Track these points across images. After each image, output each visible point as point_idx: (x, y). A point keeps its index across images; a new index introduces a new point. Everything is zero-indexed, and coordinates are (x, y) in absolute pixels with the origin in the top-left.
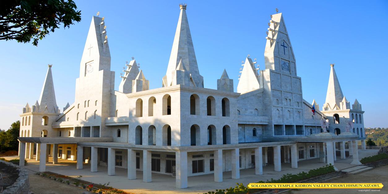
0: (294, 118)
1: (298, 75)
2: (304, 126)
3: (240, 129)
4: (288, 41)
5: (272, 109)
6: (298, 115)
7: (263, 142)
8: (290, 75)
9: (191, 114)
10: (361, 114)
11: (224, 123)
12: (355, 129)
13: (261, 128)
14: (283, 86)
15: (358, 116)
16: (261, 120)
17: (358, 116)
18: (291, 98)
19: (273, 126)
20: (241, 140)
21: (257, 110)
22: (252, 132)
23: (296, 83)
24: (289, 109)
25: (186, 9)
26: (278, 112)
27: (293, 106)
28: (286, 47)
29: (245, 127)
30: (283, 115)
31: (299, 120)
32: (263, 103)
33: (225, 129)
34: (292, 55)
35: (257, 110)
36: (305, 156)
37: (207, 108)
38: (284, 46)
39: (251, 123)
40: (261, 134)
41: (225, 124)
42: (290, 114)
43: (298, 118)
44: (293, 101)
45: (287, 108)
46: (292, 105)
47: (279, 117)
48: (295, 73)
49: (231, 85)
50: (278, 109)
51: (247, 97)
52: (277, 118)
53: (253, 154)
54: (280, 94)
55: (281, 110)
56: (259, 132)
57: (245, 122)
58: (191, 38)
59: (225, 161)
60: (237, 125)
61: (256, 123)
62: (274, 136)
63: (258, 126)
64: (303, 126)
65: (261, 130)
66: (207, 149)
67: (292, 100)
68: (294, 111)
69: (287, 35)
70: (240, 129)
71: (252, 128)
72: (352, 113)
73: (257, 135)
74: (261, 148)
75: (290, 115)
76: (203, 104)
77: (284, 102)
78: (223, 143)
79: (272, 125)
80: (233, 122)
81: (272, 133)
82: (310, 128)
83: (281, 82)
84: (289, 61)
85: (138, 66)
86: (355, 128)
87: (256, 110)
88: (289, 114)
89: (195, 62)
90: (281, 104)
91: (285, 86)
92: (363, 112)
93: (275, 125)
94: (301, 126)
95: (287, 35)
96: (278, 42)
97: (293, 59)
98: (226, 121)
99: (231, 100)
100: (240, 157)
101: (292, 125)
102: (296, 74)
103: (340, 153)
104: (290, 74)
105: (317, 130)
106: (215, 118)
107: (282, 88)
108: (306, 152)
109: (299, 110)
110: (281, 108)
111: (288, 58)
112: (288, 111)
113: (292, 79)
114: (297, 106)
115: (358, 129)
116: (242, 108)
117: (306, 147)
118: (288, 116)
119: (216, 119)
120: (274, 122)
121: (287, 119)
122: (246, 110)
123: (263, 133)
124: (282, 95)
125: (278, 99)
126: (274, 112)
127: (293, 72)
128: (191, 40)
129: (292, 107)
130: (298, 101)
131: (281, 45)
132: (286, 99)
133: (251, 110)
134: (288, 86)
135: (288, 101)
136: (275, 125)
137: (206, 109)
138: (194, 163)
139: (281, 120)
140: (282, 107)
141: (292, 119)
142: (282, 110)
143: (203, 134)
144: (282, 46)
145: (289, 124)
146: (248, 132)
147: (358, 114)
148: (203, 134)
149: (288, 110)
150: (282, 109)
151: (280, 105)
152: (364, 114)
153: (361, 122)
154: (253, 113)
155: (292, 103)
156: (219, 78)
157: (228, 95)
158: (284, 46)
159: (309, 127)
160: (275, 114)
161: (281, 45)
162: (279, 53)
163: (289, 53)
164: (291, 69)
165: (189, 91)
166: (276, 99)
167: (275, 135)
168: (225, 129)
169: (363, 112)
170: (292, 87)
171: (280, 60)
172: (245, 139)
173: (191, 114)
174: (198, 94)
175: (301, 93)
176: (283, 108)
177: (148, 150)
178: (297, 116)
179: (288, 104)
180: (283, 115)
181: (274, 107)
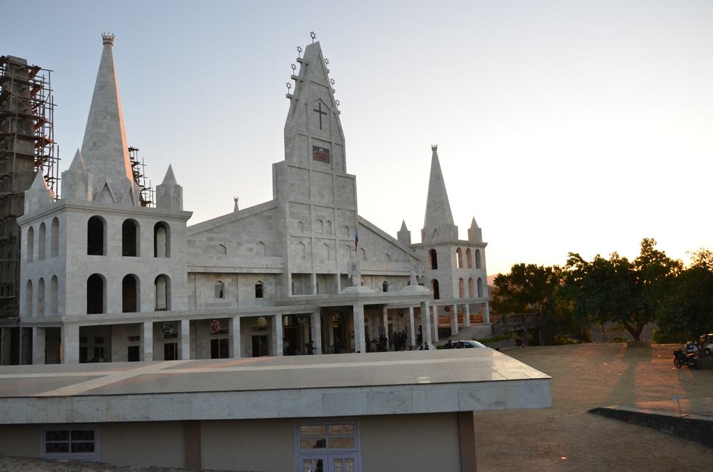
0: (338, 259)
1: (350, 170)
4: (330, 101)
5: (289, 242)
6: (349, 253)
8: (330, 172)
9: (89, 254)
10: (480, 249)
11: (158, 270)
12: (464, 281)
13: (272, 280)
16: (267, 265)
18: (331, 219)
19: (290, 276)
20: (231, 306)
23: (344, 187)
24: (327, 242)
26: (302, 247)
27: (335, 235)
32: (276, 230)
33: (130, 283)
37: (121, 242)
38: (321, 112)
40: (274, 292)
42: (328, 250)
44: (336, 225)
45: (322, 240)
46: (333, 232)
47: (304, 257)
48: (341, 167)
49: (176, 196)
52: (299, 261)
53: (134, 344)
54: (306, 212)
56: (269, 289)
57: (232, 269)
58: (117, 104)
59: (196, 347)
60: (186, 275)
62: (290, 295)
65: (274, 284)
66: (121, 319)
67: (333, 224)
68: (337, 245)
69: (328, 88)
71: (254, 281)
72: (457, 247)
73: (265, 295)
74: (239, 319)
75: (329, 254)
76: (115, 234)
77: (316, 227)
78: (122, 311)
79: (287, 275)
80: (176, 267)
81: (288, 290)
82: (383, 280)
83: (309, 186)
86: (463, 278)
88: (327, 252)
89: (119, 151)
91: (319, 194)
92: (485, 245)
93: (293, 274)
95: (328, 88)
96: (306, 104)
97: (340, 139)
98: (96, 264)
100: (366, 328)
101: (331, 273)
102: (344, 168)
103: (451, 331)
104: (332, 169)
105: (400, 283)
106: (139, 262)
107: (312, 198)
108: (374, 330)
109: (348, 243)
112: (324, 246)
113: (335, 180)
114: (344, 235)
117: (373, 319)
118: (325, 256)
119: (140, 263)
120: (292, 269)
121: (322, 262)
122: (239, 244)
124: (310, 213)
125: (303, 222)
126: (292, 248)
127: (337, 164)
128: (117, 109)
130: (347, 224)
132: (322, 221)
133: (250, 246)
135: (326, 224)
136: (293, 274)
137: (121, 245)
138: (255, 339)
139: (308, 265)
140: (311, 238)
141: (332, 262)
142: (310, 243)
143: (114, 294)
144: (315, 112)
145: (326, 273)
147: (473, 250)
148: (114, 294)
149: (325, 244)
150: (311, 242)
151: (306, 233)
152: (486, 249)
153: (478, 266)
156: (469, 227)
157: (165, 216)
158: (321, 112)
159: (379, 278)
161: (315, 110)
162: (307, 126)
163: (330, 126)
164: (333, 159)
165: (85, 209)
166: (298, 221)
167: (293, 294)
168: (130, 283)
169: (485, 245)
170: (333, 197)
171: (310, 140)
172: (238, 304)
173: (89, 254)
174: (104, 216)
175: (353, 208)
176: (314, 240)
177: (40, 326)
178: (343, 255)
179: (325, 230)
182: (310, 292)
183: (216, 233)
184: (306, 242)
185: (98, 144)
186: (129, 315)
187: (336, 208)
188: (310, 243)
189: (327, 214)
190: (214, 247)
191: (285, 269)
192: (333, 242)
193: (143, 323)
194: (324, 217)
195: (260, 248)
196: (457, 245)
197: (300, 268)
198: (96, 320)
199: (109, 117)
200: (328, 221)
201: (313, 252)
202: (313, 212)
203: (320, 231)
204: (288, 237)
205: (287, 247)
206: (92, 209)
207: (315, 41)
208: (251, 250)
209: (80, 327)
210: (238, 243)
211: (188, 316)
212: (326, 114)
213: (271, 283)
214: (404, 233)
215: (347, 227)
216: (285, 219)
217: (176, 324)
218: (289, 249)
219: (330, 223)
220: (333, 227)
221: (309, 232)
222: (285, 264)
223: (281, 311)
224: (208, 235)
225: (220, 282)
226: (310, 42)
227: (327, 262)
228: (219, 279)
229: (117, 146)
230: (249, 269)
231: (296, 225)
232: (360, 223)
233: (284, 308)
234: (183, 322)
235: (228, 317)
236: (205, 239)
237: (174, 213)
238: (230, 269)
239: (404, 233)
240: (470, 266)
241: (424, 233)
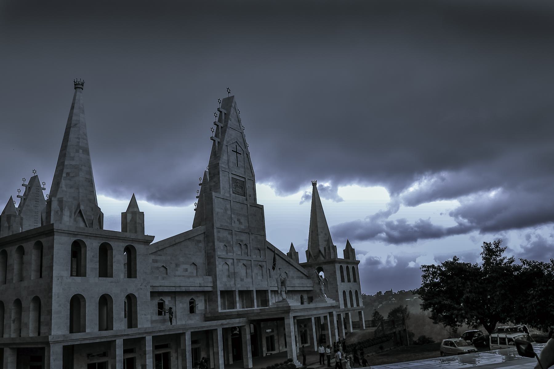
2: (269, 292)
3: (169, 301)
5: (217, 263)
7: (254, 328)
8: (245, 202)
10: (355, 266)
13: (202, 298)
14: (235, 222)
15: (351, 270)
17: (351, 270)
19: (219, 293)
21: (196, 265)
22: (187, 306)
24: (245, 262)
25: (83, 89)
26: (227, 267)
28: (241, 154)
29: (176, 297)
30: (234, 273)
31: (262, 281)
33: (131, 299)
34: (249, 167)
35: (195, 266)
36: (276, 346)
38: (237, 153)
39: (183, 289)
41: (129, 292)
43: (260, 278)
44: (251, 248)
46: (249, 254)
47: (229, 276)
50: (226, 263)
51: (178, 243)
52: (225, 279)
54: (229, 237)
55: (231, 265)
56: (200, 306)
60: (149, 294)
61: (192, 289)
63: (198, 295)
64: (268, 290)
66: (97, 338)
69: (242, 133)
70: (169, 301)
71: (187, 299)
77: (236, 249)
80: (141, 287)
84: (245, 178)
85: (42, 186)
87: (193, 266)
90: (232, 254)
94: (266, 292)
97: (251, 175)
98: (132, 287)
99: (140, 248)
102: (255, 199)
104: (247, 200)
106: (111, 282)
110: (231, 261)
111: (243, 173)
112: (243, 265)
115: (350, 292)
116: (171, 263)
120: (220, 287)
121: (242, 280)
122: (177, 265)
123: (206, 308)
126: (220, 267)
129: (249, 258)
130: (259, 247)
131: (232, 151)
132: (240, 245)
134: (242, 221)
135: (243, 247)
139: (232, 283)
141: (249, 280)
146: (181, 305)
147: (350, 267)
149: (243, 264)
154: (189, 270)
155: (249, 251)
157: (133, 240)
158: (237, 153)
160: (222, 271)
166: (223, 244)
168: (131, 299)
174: (84, 240)
176: (235, 261)
180: (234, 272)
181: (221, 259)
182: (252, 306)
183: (160, 255)
184: (230, 262)
185: (71, 175)
186: (104, 333)
187: (250, 233)
188: (233, 264)
189: (244, 237)
190: (158, 268)
191: (215, 286)
192: (249, 263)
193: (116, 340)
194: (242, 241)
195: (191, 269)
196: (340, 263)
197: (226, 285)
198: (78, 338)
199: (81, 151)
200: (245, 244)
201: (235, 271)
202: (234, 236)
203: (239, 253)
204: (217, 258)
205: (216, 268)
206: (75, 233)
207: (230, 95)
208: (186, 270)
209: (63, 346)
210: (176, 265)
211: (151, 333)
212: (241, 154)
213: (201, 300)
214: (293, 253)
215: (258, 249)
216: (214, 242)
217: (141, 341)
218: (217, 269)
219: (247, 246)
220: (249, 249)
221: (232, 254)
222: (215, 282)
223: (222, 324)
224: (153, 257)
225: (162, 300)
226: (226, 96)
227: (245, 280)
228: (161, 298)
229: (88, 177)
230: (186, 288)
231: (222, 248)
232: (268, 248)
233: (224, 322)
234: (117, 342)
235: (181, 332)
236: (151, 261)
237: (140, 237)
238: (172, 288)
239: (293, 253)
240: (349, 281)
241: (308, 252)
